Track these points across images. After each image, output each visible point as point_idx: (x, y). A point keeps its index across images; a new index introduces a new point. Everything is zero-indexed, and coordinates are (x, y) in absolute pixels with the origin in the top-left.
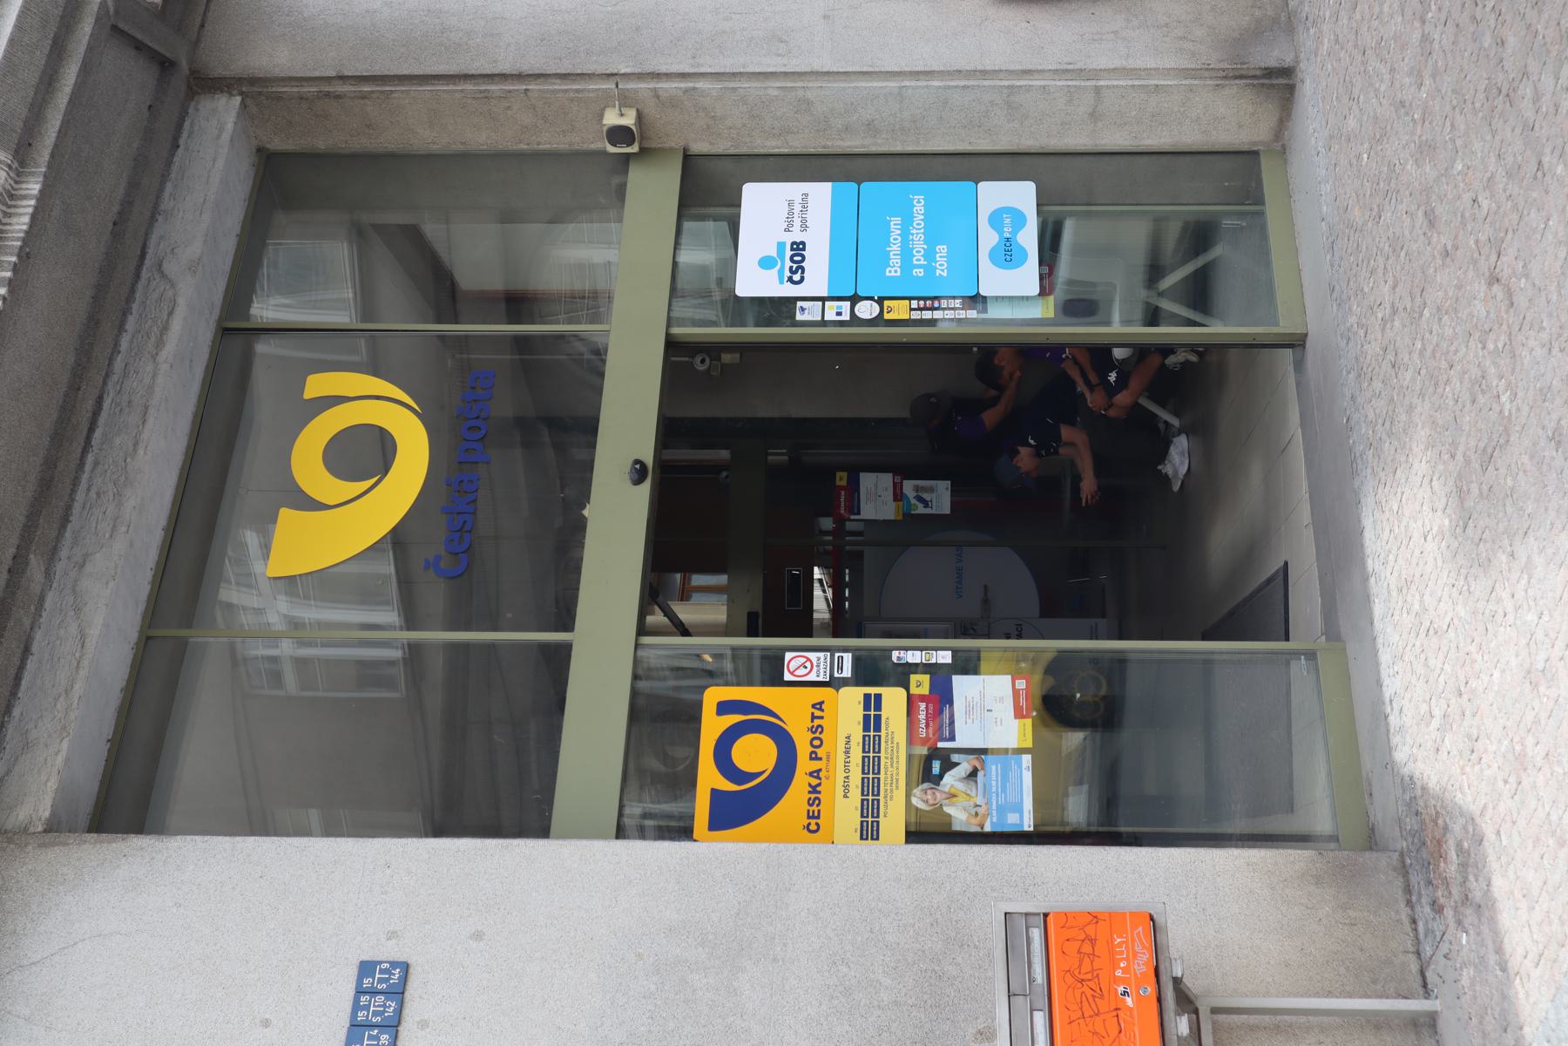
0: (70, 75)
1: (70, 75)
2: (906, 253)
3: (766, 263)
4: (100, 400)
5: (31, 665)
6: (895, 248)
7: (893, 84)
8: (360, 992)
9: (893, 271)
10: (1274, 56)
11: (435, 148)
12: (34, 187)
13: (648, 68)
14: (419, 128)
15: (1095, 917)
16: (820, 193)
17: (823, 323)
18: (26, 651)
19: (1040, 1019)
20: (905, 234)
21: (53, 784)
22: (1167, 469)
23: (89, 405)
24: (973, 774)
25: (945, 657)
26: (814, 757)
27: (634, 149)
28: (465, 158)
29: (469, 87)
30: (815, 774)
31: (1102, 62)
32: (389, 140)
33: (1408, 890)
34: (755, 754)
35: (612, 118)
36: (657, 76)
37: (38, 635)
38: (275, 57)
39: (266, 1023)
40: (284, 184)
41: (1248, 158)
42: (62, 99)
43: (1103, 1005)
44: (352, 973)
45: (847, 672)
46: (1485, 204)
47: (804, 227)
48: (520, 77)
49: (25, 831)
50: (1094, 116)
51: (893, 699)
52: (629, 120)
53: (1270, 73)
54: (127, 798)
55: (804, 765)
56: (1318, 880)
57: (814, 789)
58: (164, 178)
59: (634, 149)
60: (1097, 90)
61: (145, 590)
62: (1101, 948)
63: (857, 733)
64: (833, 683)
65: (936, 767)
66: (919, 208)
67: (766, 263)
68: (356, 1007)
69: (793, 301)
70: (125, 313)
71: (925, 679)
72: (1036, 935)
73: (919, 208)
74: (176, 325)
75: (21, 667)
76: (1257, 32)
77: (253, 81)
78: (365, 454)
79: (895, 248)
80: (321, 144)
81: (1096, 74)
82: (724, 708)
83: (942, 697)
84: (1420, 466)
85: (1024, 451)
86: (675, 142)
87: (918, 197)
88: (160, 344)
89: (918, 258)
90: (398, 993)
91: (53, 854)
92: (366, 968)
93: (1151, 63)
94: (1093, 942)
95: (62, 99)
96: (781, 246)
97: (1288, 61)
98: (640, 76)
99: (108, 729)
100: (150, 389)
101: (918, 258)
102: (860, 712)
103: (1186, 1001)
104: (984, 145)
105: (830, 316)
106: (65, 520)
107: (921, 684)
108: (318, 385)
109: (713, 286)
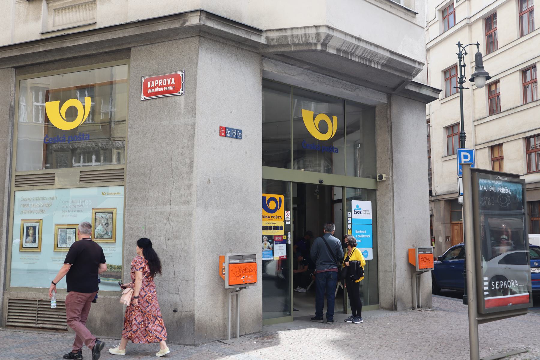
0: (398, 74)
1: (398, 74)
2: (360, 234)
3: (357, 206)
4: (335, 77)
5: (290, 66)
6: (360, 232)
7: (392, 231)
8: (237, 130)
9: (357, 232)
10: (399, 307)
11: (377, 141)
12: (379, 68)
13: (394, 183)
14: (381, 138)
15: (256, 272)
16: (370, 217)
17: (347, 218)
18: (293, 65)
19: (238, 261)
20: (363, 234)
21: (270, 70)
22: (298, 288)
23: (335, 76)
24: (269, 248)
25: (289, 242)
26: (272, 217)
27: (378, 180)
28: (374, 147)
29: (390, 148)
30: (269, 217)
31: (397, 272)
32: (378, 132)
33: (256, 333)
34: (272, 205)
35: (384, 176)
36: (393, 184)
37: (294, 67)
38: (395, 110)
39: (231, 112)
40: (369, 111)
41: (378, 302)
42: (394, 72)
43: (241, 273)
44: (240, 129)
45: (287, 223)
46: (393, 344)
47: (364, 214)
48: (392, 158)
49: (262, 66)
50: (386, 271)
51: (282, 232)
52: (384, 179)
53: (396, 306)
54: (269, 85)
55: (271, 215)
56: (257, 315)
57: (266, 217)
58: (373, 89)
59: (378, 180)
60: (392, 272)
61: (305, 87)
62: (251, 273)
63: (276, 225)
64: (285, 221)
65: (270, 241)
66: (367, 236)
67: (357, 206)
68: (234, 129)
69: (351, 211)
70: (350, 82)
71: (285, 239)
72: (252, 260)
73: (367, 236)
74: (348, 92)
75: (290, 64)
76: (403, 303)
77: (390, 106)
78: (323, 128)
79: (360, 232)
80: (377, 118)
81: (395, 271)
82: (280, 199)
83: (283, 242)
84: (344, 334)
85: (302, 258)
86: (378, 187)
87: (369, 236)
88: (344, 89)
89: (359, 236)
90: (237, 137)
91: (259, 71)
92: (241, 131)
93: (397, 282)
94: (252, 271)
95: (394, 72)
96: (360, 209)
97: (398, 309)
98: (393, 181)
99: (275, 80)
100: (336, 87)
101: (359, 236)
102: (280, 226)
103: (241, 289)
104: (379, 249)
105: (349, 219)
106: (314, 71)
107: (285, 238)
108: (335, 118)
109: (114, 165)
